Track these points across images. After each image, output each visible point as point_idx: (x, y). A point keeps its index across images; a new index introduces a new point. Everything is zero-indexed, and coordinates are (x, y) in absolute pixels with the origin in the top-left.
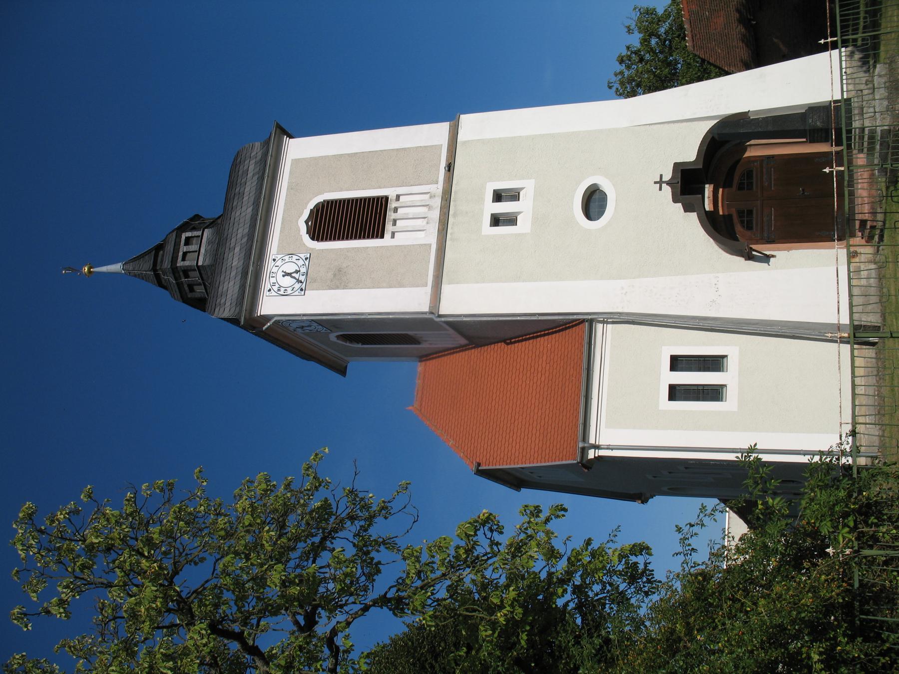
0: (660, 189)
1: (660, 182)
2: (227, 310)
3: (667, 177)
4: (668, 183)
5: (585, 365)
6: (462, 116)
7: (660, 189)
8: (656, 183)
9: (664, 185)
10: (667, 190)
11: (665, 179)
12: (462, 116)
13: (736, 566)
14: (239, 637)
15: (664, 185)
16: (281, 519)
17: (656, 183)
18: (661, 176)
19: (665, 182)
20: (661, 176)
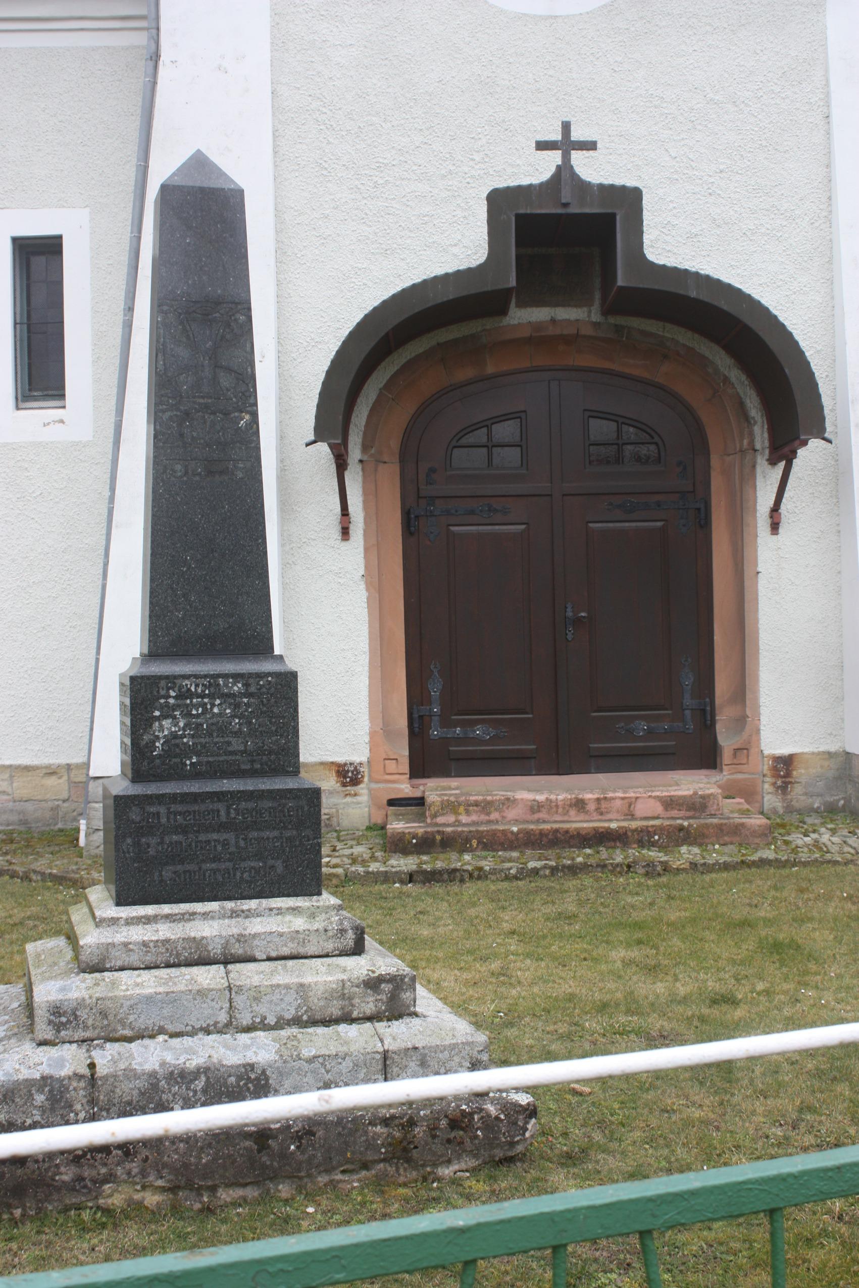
0: (542, 146)
1: (566, 144)
2: (403, 786)
3: (591, 169)
4: (564, 172)
5: (19, 376)
6: (572, 139)
7: (542, 146)
8: (566, 127)
9: (554, 158)
10: (539, 169)
11: (578, 159)
12: (572, 139)
13: (391, 872)
14: (794, 864)
15: (554, 158)
16: (177, 750)
17: (566, 127)
18: (591, 146)
19: (566, 157)
20: (591, 146)
